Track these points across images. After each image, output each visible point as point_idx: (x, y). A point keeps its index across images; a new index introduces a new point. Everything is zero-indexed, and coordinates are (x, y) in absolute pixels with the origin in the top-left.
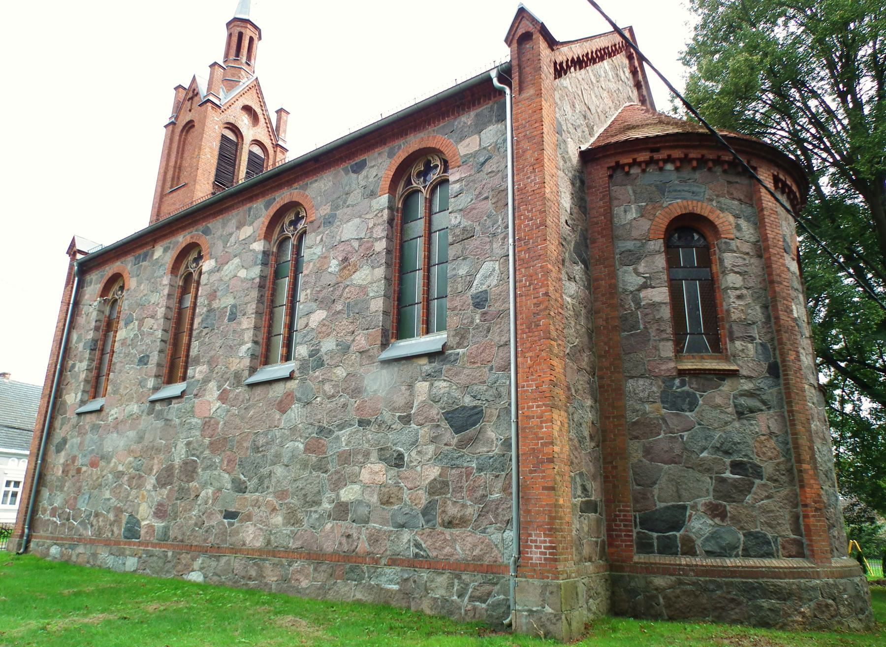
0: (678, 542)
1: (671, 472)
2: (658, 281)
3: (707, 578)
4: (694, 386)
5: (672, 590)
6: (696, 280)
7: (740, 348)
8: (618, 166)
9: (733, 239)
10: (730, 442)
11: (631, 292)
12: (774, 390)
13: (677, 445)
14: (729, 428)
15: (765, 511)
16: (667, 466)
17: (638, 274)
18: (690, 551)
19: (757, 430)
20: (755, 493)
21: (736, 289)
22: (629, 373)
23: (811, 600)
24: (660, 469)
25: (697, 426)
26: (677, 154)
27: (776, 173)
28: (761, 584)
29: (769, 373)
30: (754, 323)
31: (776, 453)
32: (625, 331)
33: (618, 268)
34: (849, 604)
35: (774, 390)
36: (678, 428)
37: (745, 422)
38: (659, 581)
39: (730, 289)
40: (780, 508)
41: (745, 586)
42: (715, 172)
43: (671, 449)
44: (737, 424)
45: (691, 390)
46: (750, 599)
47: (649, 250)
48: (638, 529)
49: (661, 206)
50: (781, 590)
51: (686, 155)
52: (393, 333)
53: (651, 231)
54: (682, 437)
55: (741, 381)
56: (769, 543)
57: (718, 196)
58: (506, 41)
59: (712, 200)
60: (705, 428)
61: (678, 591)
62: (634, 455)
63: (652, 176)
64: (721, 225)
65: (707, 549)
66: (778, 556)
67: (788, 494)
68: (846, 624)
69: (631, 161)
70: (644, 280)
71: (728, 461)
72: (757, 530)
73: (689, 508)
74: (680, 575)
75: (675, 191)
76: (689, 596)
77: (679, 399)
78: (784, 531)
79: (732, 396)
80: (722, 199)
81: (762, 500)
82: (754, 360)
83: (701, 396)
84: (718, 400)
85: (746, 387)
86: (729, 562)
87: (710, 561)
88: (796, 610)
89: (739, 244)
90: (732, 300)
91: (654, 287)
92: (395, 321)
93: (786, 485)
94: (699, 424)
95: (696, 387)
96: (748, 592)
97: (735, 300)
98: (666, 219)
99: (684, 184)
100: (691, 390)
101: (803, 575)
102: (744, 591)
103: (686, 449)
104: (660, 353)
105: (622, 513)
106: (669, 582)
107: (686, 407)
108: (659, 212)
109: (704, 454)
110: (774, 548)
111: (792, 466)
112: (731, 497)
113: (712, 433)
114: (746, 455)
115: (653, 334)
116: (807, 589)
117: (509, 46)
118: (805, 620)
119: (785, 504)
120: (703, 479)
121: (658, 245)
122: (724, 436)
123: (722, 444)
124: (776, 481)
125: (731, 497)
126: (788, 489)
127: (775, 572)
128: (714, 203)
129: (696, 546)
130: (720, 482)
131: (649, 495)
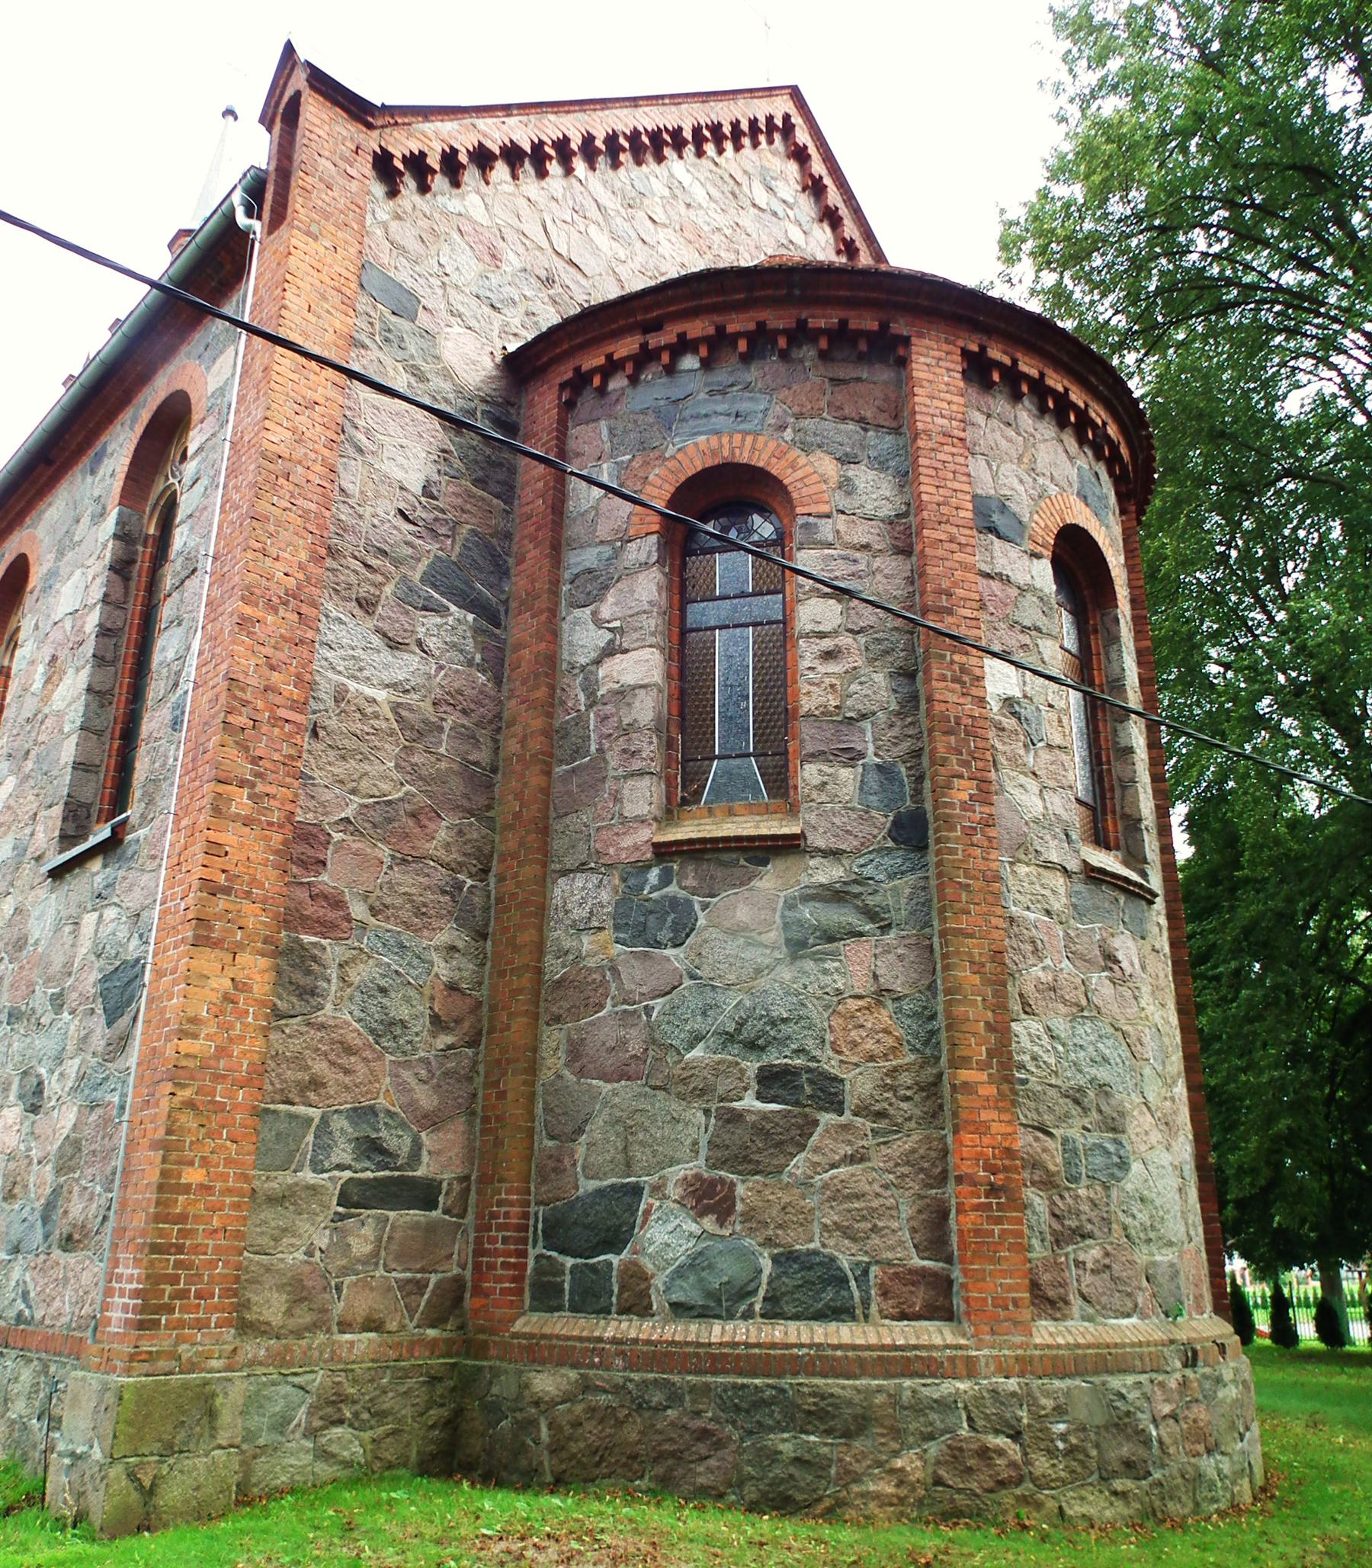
0: (614, 1280)
1: (617, 1100)
2: (635, 636)
3: (651, 1376)
4: (690, 882)
5: (568, 1405)
6: (747, 625)
7: (816, 780)
8: (579, 382)
9: (828, 516)
10: (762, 1017)
11: (583, 668)
12: (906, 884)
13: (634, 1032)
14: (763, 983)
15: (837, 1195)
16: (609, 1086)
17: (598, 623)
18: (638, 1305)
19: (840, 985)
20: (816, 1150)
21: (822, 635)
22: (560, 862)
23: (931, 1437)
24: (594, 1095)
25: (687, 982)
26: (698, 328)
27: (975, 348)
28: (783, 1391)
29: (894, 840)
30: (864, 717)
31: (890, 1041)
32: (561, 762)
33: (564, 614)
34: (1071, 1451)
35: (906, 884)
36: (644, 989)
37: (809, 965)
38: (546, 1383)
39: (807, 636)
40: (886, 1187)
41: (741, 1398)
42: (801, 361)
43: (623, 1043)
44: (786, 974)
45: (683, 894)
46: (750, 1433)
47: (627, 564)
48: (540, 1250)
49: (662, 458)
50: (835, 1406)
51: (720, 330)
52: (100, 811)
53: (633, 518)
54: (648, 1010)
55: (812, 863)
56: (843, 1281)
57: (798, 416)
58: (262, 121)
59: (782, 428)
60: (705, 986)
61: (579, 1408)
62: (550, 1062)
63: (655, 389)
64: (799, 485)
65: (674, 1298)
66: (866, 1317)
67: (913, 1151)
68: (1051, 1504)
69: (601, 360)
70: (609, 636)
71: (751, 1066)
72: (812, 1246)
73: (646, 1192)
74: (592, 1366)
75: (697, 417)
76: (601, 1421)
77: (651, 918)
78: (892, 1248)
79: (782, 900)
80: (805, 423)
81: (833, 1166)
82: (852, 809)
83: (705, 906)
84: (743, 914)
85: (822, 878)
86: (717, 1332)
87: (690, 1331)
88: (879, 1464)
89: (842, 527)
90: (806, 663)
91: (626, 651)
92: (109, 784)
93: (913, 1125)
94: (693, 977)
95: (695, 884)
96: (747, 1411)
97: (816, 663)
98: (667, 486)
99: (719, 397)
100: (683, 894)
101: (917, 1366)
102: (737, 1409)
103: (654, 1041)
104: (621, 808)
105: (503, 1210)
106: (565, 1386)
107: (664, 935)
108: (657, 471)
109: (697, 1052)
110: (856, 1294)
111: (940, 1075)
112: (750, 1162)
113: (720, 998)
114: (800, 1051)
115: (613, 764)
116: (919, 1407)
117: (269, 130)
118: (903, 1492)
119: (903, 1176)
120: (688, 1115)
121: (645, 549)
122: (748, 1004)
123: (741, 1024)
124: (881, 1115)
125: (750, 1162)
126: (915, 1137)
127: (834, 1359)
128: (788, 434)
129: (652, 1291)
130: (728, 1121)
131: (567, 1162)
